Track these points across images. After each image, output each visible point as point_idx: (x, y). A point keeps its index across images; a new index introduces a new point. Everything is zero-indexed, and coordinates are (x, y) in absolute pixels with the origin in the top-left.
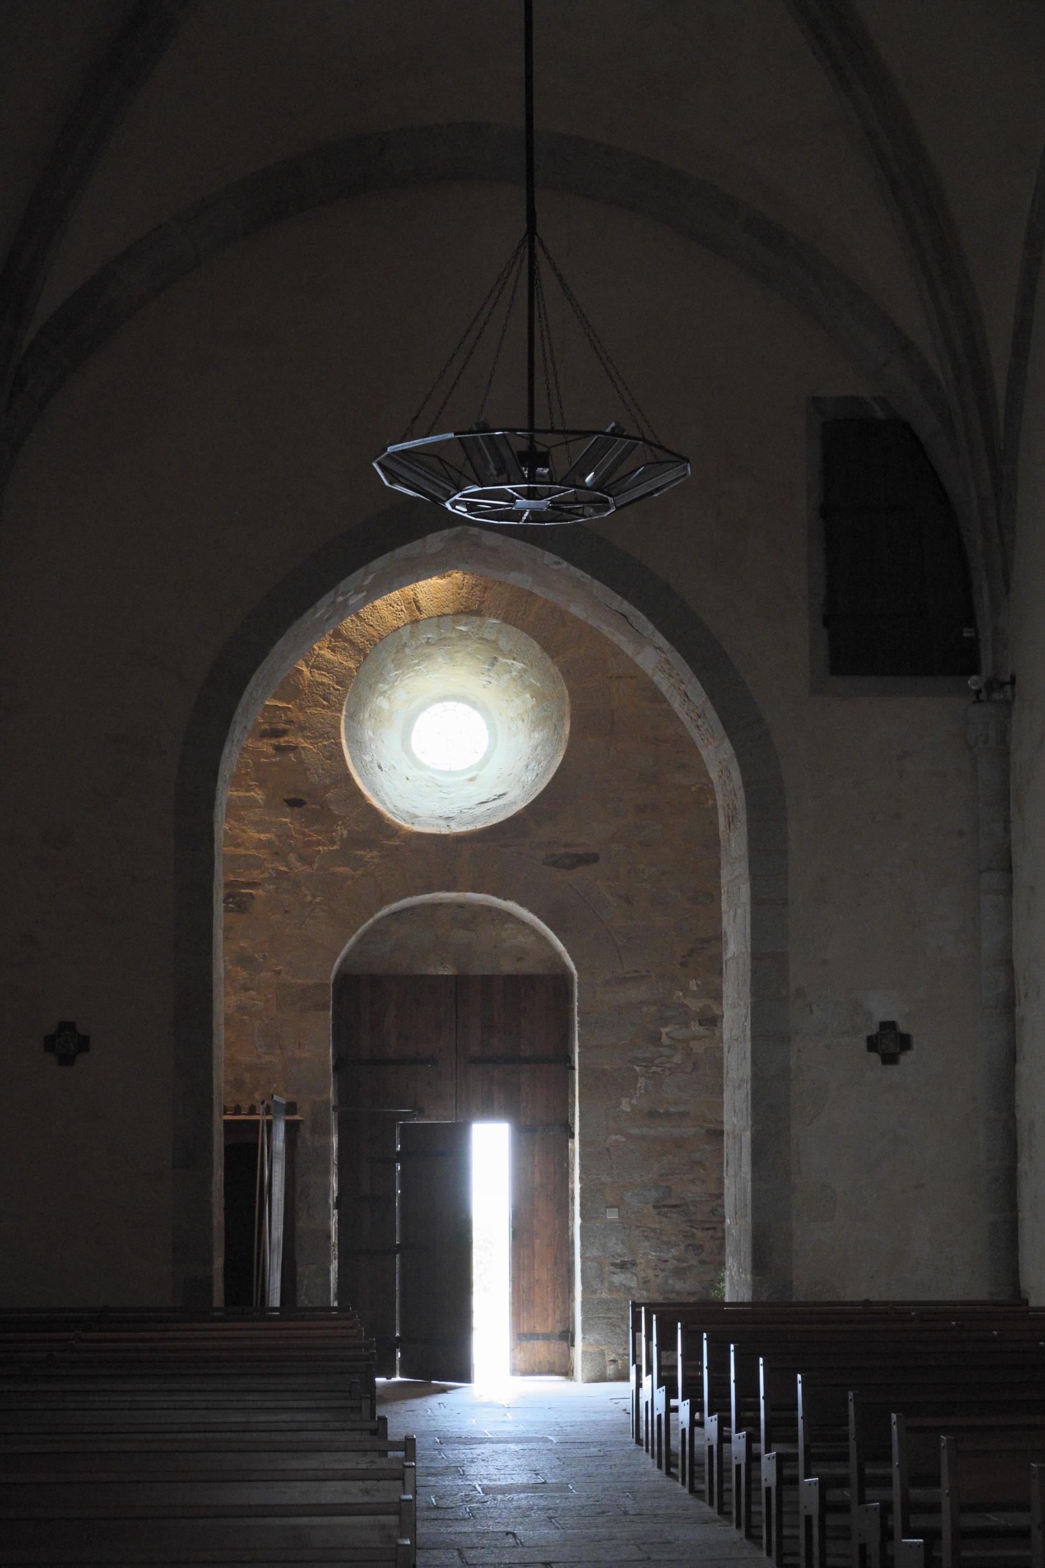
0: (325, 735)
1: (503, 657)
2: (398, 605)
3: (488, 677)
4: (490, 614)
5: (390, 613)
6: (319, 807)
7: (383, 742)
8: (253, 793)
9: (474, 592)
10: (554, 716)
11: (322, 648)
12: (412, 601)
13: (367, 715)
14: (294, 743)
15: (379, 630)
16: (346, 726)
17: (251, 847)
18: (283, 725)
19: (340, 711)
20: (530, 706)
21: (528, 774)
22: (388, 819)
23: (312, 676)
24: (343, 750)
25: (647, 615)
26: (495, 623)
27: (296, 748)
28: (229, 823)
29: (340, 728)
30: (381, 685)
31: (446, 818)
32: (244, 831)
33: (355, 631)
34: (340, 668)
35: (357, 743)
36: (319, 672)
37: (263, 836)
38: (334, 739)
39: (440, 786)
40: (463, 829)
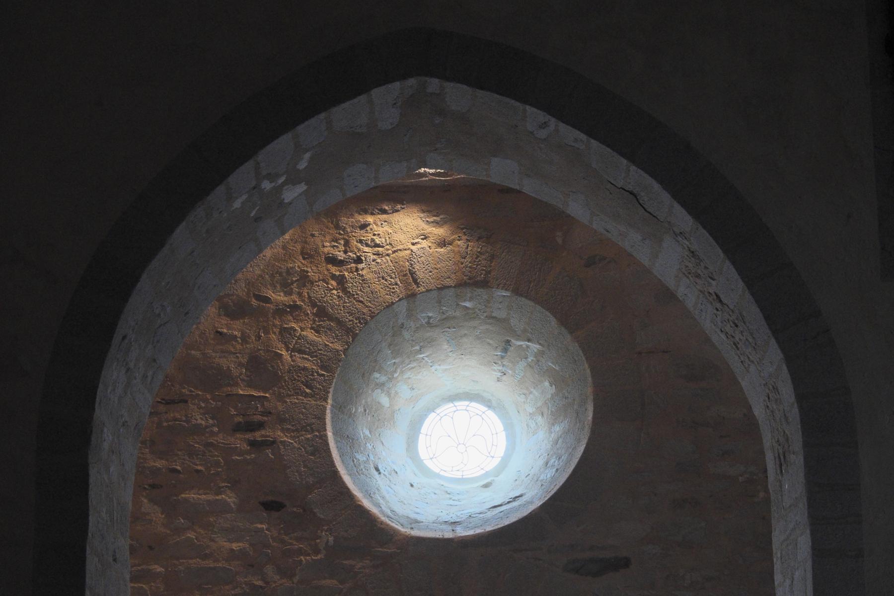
0: (308, 428)
1: (517, 340)
2: (391, 278)
3: (501, 367)
4: (498, 285)
5: (382, 287)
6: (301, 511)
7: (383, 444)
8: (223, 496)
9: (480, 261)
10: (576, 403)
11: (304, 328)
12: (408, 273)
13: (361, 409)
14: (272, 438)
15: (370, 307)
16: (332, 418)
17: (221, 559)
18: (259, 418)
19: (326, 400)
20: (550, 396)
21: (547, 471)
22: (382, 523)
23: (293, 361)
24: (328, 444)
25: (661, 182)
26: (504, 296)
27: (274, 442)
28: (196, 532)
29: (325, 419)
30: (377, 375)
31: (452, 523)
32: (212, 540)
33: (342, 309)
34: (326, 350)
35: (349, 440)
36: (301, 356)
37: (235, 546)
38: (318, 431)
39: (449, 494)
40: (471, 533)
